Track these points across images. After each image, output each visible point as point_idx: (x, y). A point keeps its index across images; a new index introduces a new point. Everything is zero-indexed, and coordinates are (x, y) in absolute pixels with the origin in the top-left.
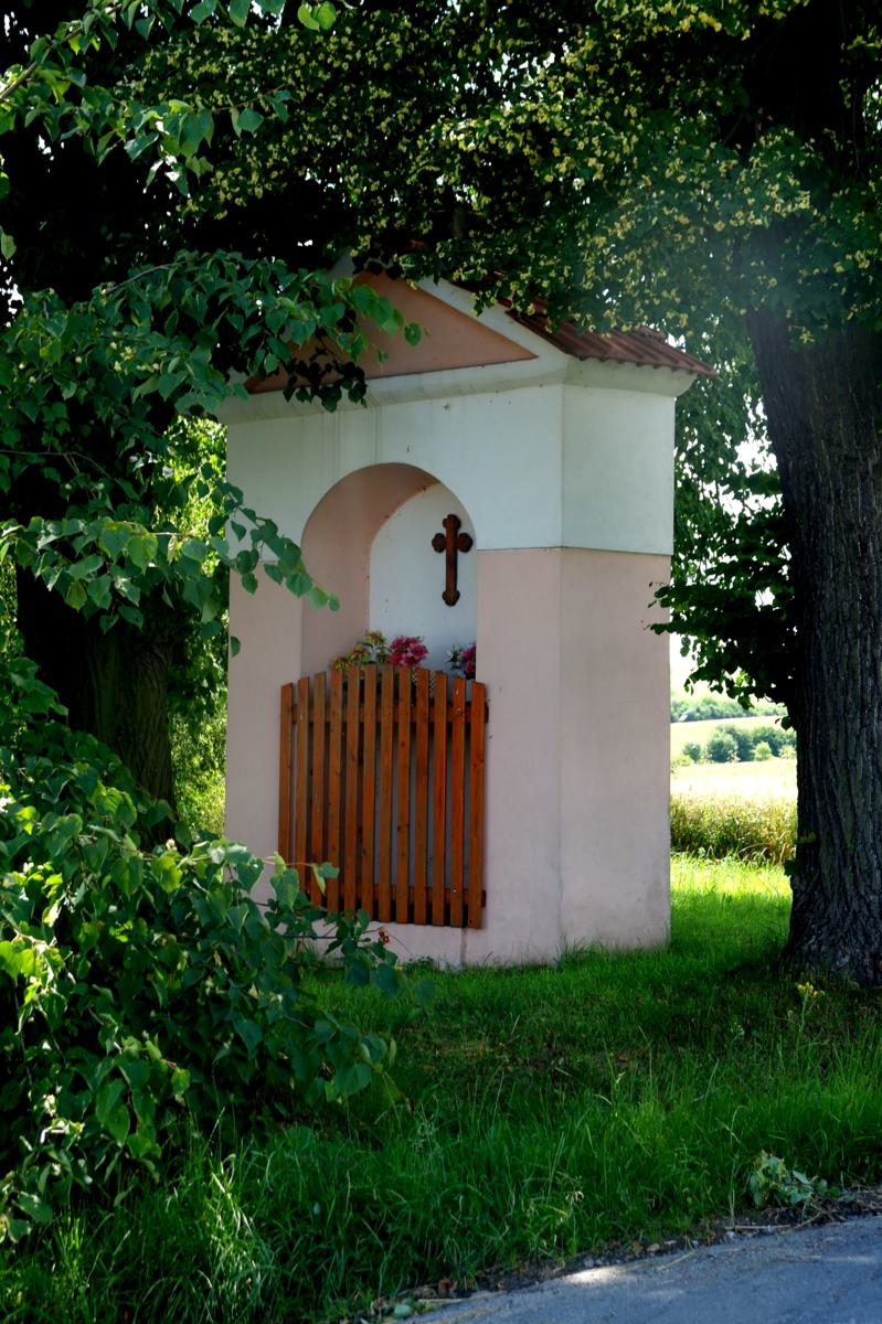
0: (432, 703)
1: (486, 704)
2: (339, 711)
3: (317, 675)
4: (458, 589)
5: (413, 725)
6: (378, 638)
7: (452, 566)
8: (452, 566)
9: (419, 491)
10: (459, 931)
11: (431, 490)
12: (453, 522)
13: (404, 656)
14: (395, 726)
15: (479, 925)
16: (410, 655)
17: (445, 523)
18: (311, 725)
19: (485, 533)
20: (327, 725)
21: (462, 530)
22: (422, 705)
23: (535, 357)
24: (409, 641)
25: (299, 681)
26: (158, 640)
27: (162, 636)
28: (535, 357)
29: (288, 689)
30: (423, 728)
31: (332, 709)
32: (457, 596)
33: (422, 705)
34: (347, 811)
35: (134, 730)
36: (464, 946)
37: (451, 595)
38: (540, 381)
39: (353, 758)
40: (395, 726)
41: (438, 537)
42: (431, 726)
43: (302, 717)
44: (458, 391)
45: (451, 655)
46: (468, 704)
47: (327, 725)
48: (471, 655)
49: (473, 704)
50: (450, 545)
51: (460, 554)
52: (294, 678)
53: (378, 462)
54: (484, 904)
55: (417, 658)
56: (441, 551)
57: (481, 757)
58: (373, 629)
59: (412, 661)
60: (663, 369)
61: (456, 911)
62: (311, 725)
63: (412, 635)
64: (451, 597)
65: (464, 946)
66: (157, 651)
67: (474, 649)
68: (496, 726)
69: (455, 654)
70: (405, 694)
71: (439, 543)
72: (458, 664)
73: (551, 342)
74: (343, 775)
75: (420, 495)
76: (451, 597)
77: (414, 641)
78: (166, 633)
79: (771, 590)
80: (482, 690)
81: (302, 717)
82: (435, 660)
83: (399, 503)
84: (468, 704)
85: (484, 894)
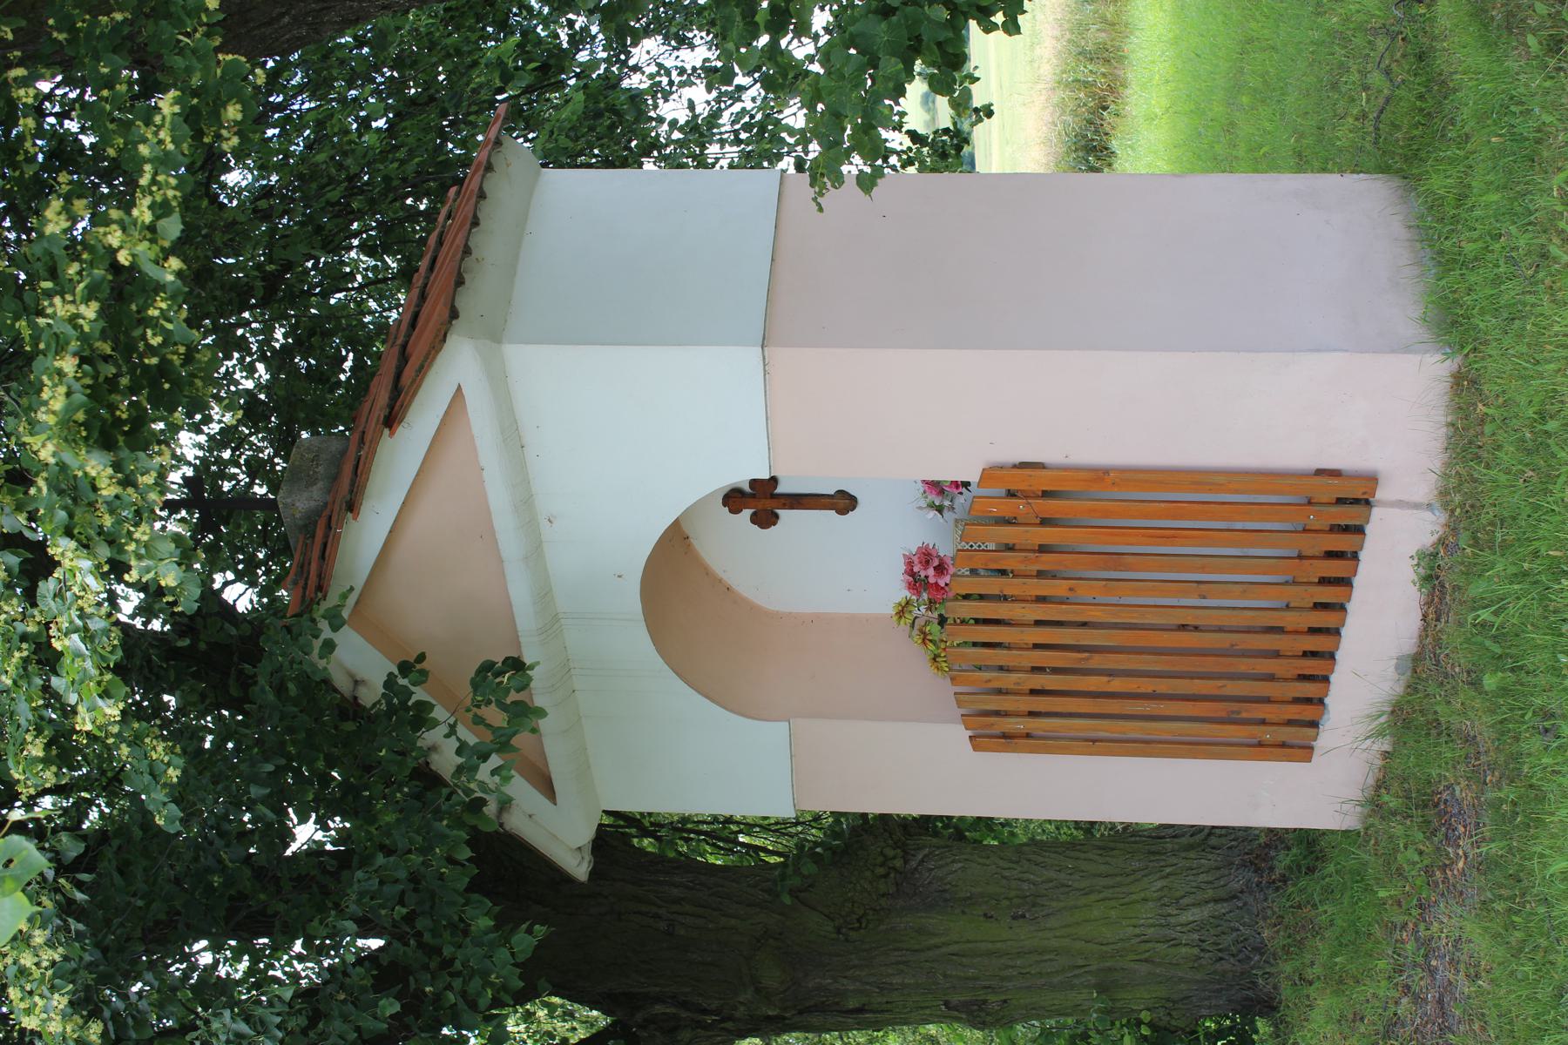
0: (1010, 548)
1: (1015, 466)
2: (1014, 676)
3: (959, 704)
4: (832, 492)
5: (1040, 574)
6: (903, 610)
7: (799, 501)
8: (799, 501)
9: (689, 545)
10: (1376, 513)
11: (687, 528)
12: (734, 499)
13: (932, 580)
14: (1041, 599)
15: (1371, 480)
16: (931, 572)
17: (735, 510)
18: (1032, 714)
19: (748, 468)
20: (1033, 692)
21: (747, 488)
22: (1010, 561)
23: (459, 386)
24: (910, 572)
25: (967, 729)
26: (898, 863)
27: (894, 858)
28: (459, 386)
29: (977, 742)
30: (1047, 561)
31: (1012, 687)
32: (842, 493)
33: (1010, 561)
34: (1166, 668)
35: (1017, 897)
36: (1400, 504)
37: (843, 503)
38: (499, 382)
39: (1087, 659)
40: (1041, 599)
41: (755, 519)
42: (1043, 549)
43: (1019, 725)
44: (525, 504)
45: (932, 514)
46: (1011, 494)
47: (1033, 692)
48: (935, 486)
49: (1013, 487)
50: (768, 504)
51: (780, 489)
52: (961, 734)
53: (641, 617)
54: (1335, 473)
55: (936, 563)
56: (777, 516)
57: (1100, 475)
58: (890, 610)
59: (941, 569)
60: (486, 188)
61: (1346, 516)
62: (1032, 714)
63: (902, 567)
64: (844, 502)
65: (1400, 504)
66: (914, 864)
67: (925, 482)
68: (1052, 452)
69: (932, 506)
70: (994, 585)
71: (765, 519)
72: (947, 503)
73: (429, 366)
74: (1111, 673)
75: (695, 542)
76: (844, 502)
77: (910, 564)
78: (890, 852)
79: (775, 488)
80: (991, 474)
81: (1019, 725)
82: (940, 536)
83: (707, 571)
84: (1011, 494)
85: (1320, 472)
